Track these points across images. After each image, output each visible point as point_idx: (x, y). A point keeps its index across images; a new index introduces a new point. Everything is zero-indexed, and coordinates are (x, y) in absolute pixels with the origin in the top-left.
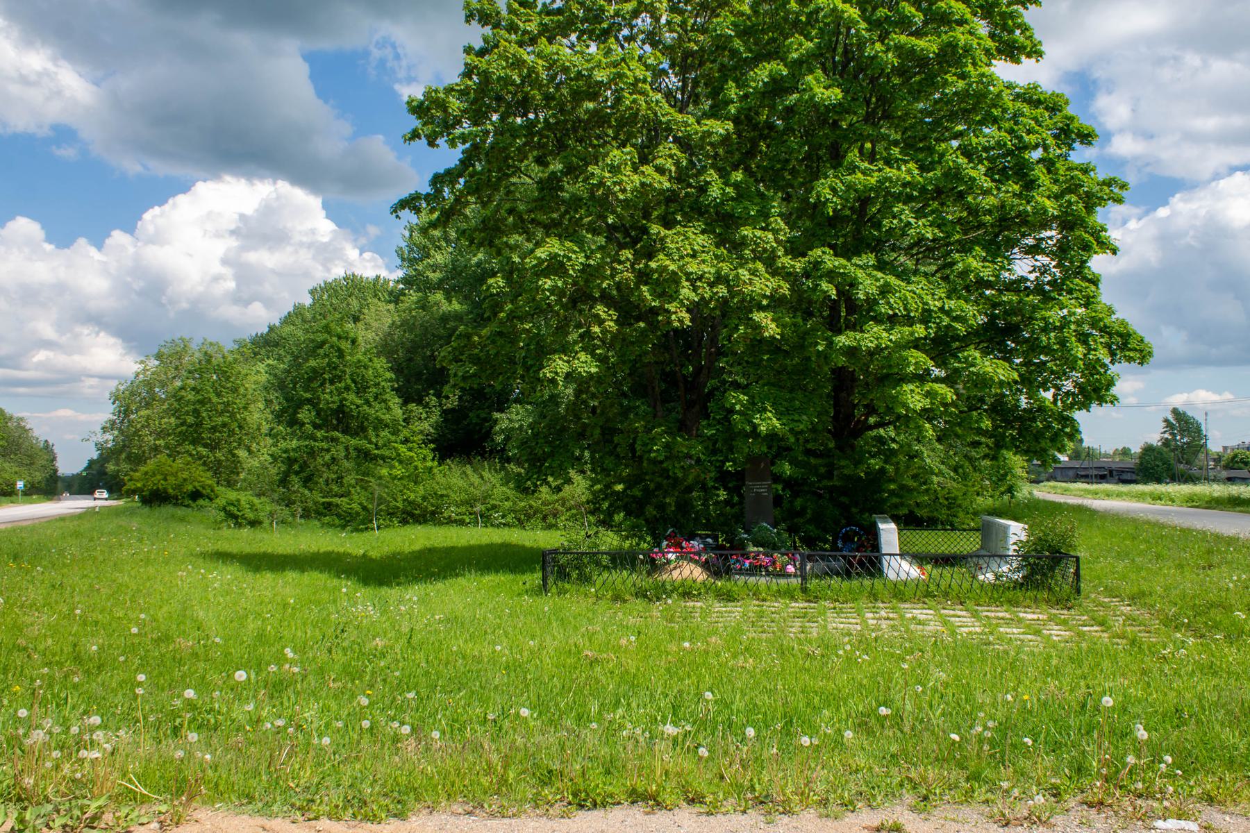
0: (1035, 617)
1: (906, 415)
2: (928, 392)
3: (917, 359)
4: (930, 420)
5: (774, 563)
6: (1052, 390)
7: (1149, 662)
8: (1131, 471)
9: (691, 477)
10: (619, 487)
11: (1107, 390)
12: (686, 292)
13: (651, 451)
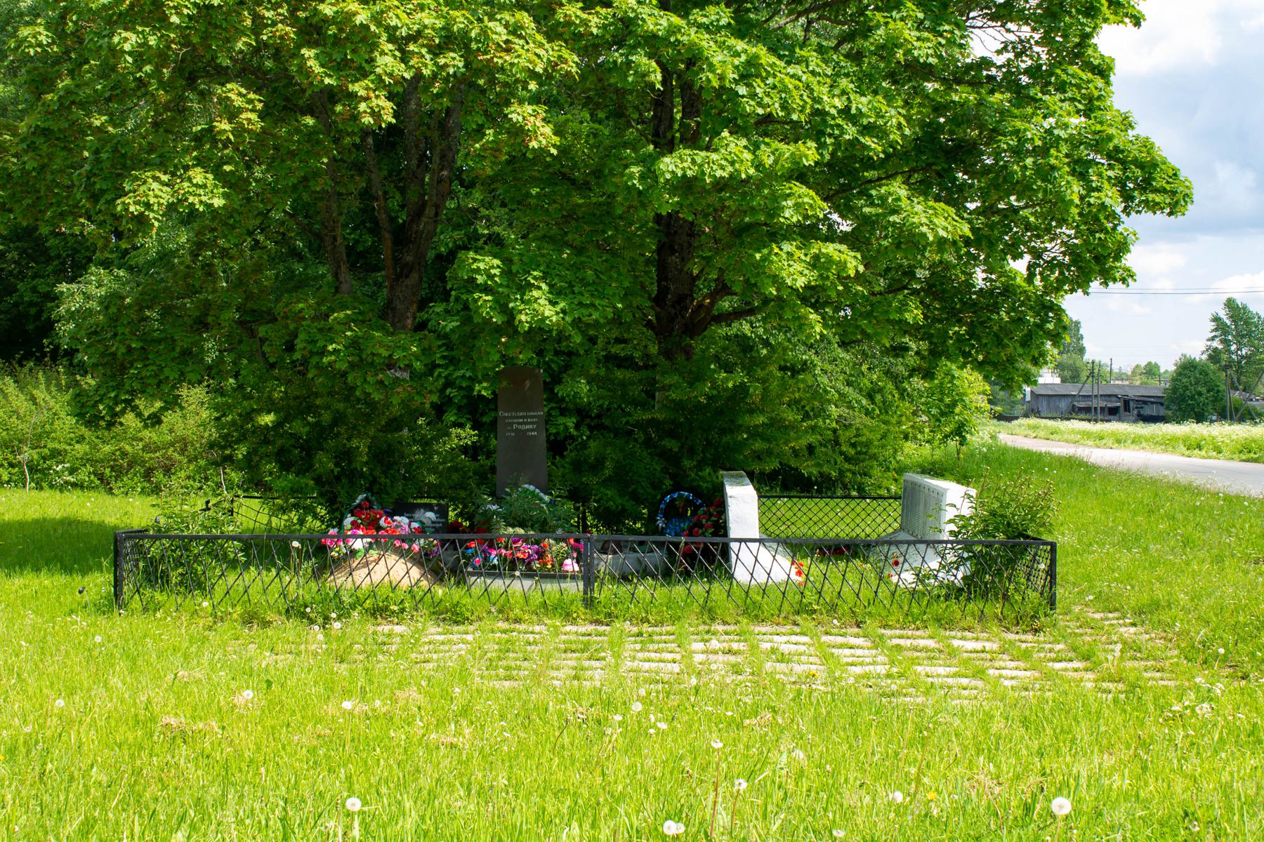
0: (978, 646)
1: (779, 298)
2: (816, 257)
3: (801, 201)
4: (816, 307)
5: (541, 555)
6: (1027, 258)
7: (1152, 728)
8: (1158, 401)
9: (395, 400)
10: (268, 419)
11: (1117, 258)
12: (387, 62)
13: (323, 352)
